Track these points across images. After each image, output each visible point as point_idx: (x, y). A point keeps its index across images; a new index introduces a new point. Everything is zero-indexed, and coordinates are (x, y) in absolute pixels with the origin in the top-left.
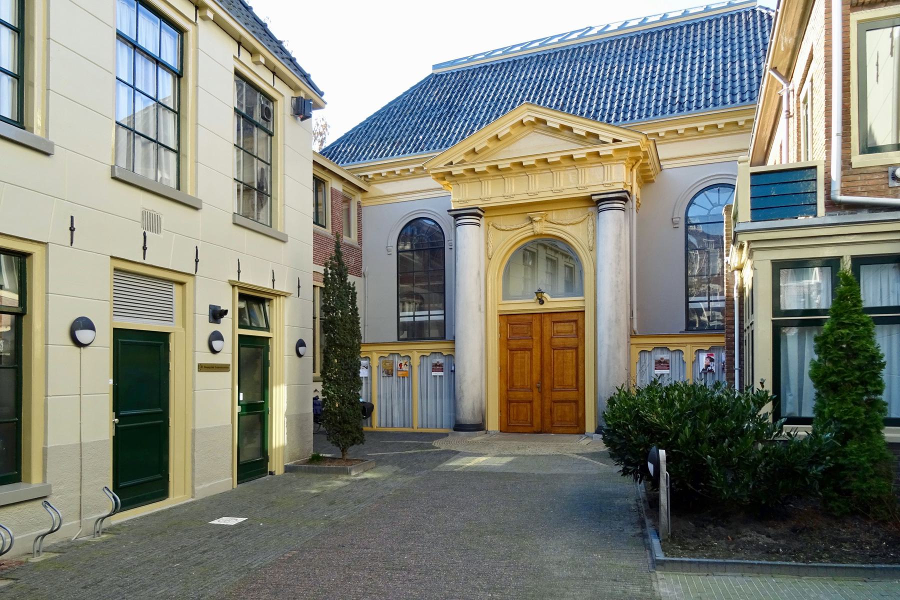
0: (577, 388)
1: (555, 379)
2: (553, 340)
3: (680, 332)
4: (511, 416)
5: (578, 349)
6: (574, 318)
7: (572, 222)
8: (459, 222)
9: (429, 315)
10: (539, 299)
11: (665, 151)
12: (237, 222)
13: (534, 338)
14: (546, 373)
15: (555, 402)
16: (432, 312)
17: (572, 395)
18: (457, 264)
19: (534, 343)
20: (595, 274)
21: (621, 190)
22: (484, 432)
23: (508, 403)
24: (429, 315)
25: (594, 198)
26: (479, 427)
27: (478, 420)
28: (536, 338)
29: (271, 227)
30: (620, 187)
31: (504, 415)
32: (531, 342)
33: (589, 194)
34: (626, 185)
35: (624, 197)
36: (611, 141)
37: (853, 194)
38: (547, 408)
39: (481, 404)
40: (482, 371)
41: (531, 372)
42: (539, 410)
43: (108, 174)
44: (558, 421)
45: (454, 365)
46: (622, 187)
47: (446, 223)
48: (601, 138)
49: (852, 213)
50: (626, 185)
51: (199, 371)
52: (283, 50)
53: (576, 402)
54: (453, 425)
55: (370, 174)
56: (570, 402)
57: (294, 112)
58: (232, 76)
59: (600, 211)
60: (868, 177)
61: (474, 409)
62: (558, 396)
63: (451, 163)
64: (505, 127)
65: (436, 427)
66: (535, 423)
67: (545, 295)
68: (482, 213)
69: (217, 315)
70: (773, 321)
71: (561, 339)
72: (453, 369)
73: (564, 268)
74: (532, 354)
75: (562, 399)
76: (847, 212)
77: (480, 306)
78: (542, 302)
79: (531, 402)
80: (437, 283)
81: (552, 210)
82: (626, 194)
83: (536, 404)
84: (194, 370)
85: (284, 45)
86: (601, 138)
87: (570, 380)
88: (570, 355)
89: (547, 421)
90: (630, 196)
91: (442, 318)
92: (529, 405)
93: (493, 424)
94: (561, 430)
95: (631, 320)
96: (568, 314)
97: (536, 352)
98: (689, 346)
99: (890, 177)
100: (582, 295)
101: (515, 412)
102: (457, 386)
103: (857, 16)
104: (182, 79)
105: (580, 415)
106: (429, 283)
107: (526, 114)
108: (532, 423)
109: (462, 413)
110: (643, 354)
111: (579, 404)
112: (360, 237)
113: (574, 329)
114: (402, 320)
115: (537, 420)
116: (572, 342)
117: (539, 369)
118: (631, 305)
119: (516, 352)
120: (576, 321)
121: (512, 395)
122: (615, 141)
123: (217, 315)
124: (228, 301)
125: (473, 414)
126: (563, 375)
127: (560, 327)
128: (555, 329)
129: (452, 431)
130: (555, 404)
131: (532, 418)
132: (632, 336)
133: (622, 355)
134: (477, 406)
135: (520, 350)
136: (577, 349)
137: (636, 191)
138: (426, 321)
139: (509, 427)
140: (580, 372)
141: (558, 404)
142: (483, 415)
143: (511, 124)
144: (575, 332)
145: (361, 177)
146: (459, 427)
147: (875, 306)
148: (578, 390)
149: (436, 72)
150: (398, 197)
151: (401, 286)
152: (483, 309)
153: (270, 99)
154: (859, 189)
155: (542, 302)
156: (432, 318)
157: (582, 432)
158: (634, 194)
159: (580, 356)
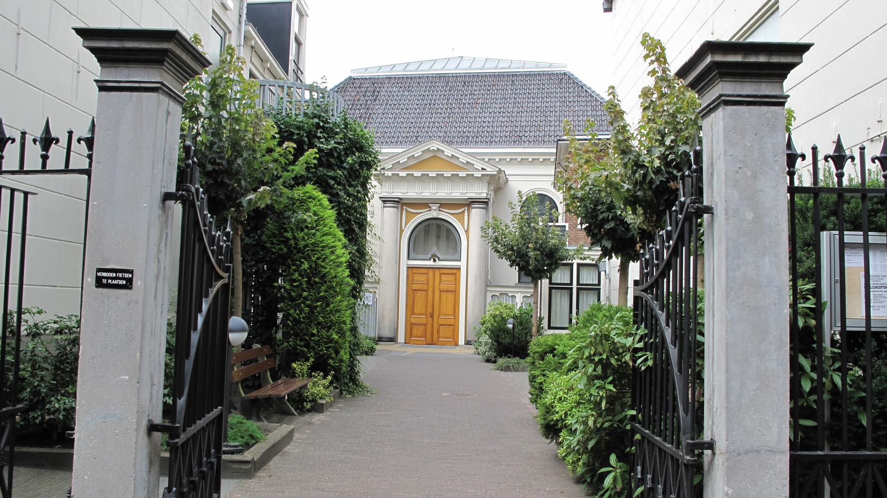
11: (508, 170)
23: (410, 328)
26: (392, 340)
30: (484, 195)
35: (485, 203)
36: (480, 169)
89: (435, 336)
93: (401, 338)
98: (519, 293)
111: (455, 327)
115: (429, 337)
121: (413, 320)
122: (483, 169)
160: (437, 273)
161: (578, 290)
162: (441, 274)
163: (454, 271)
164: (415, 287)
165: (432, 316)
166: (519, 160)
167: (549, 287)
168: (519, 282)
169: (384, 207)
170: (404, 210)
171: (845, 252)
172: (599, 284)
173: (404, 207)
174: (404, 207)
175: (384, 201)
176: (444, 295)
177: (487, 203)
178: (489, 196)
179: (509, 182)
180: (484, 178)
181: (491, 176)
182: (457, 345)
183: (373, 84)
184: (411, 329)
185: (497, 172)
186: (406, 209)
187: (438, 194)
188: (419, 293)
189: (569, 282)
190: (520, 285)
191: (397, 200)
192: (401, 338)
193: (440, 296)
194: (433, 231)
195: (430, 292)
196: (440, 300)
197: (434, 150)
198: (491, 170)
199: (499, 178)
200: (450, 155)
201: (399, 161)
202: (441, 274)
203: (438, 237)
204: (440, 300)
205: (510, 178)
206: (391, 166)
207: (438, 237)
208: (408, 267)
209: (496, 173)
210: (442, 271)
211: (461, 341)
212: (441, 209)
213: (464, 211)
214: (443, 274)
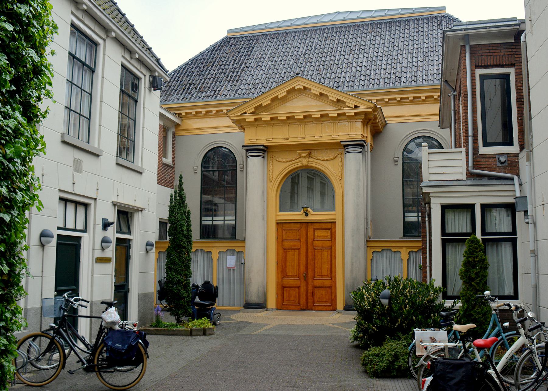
0: (331, 277)
1: (316, 271)
2: (315, 242)
3: (400, 238)
4: (285, 298)
5: (331, 249)
6: (329, 227)
7: (327, 159)
8: (347, 150)
9: (224, 220)
10: (305, 212)
11: (387, 111)
12: (119, 163)
13: (301, 240)
14: (309, 266)
15: (315, 287)
16: (226, 218)
17: (328, 283)
18: (248, 185)
19: (301, 245)
20: (343, 196)
21: (360, 139)
22: (265, 309)
23: (282, 288)
24: (224, 220)
25: (342, 143)
26: (262, 306)
27: (261, 301)
28: (303, 240)
29: (133, 162)
30: (359, 137)
31: (280, 297)
32: (299, 243)
33: (339, 141)
34: (363, 136)
35: (360, 145)
36: (353, 106)
37: (480, 169)
38: (310, 291)
39: (264, 288)
40: (264, 265)
41: (299, 266)
42: (305, 293)
43: (59, 139)
44: (318, 301)
45: (244, 259)
46: (361, 137)
47: (239, 153)
48: (347, 104)
49: (480, 179)
50: (363, 136)
51: (96, 262)
52: (152, 53)
53: (330, 287)
54: (243, 303)
55: (183, 112)
56: (326, 287)
57: (151, 85)
58: (120, 67)
59: (346, 152)
60: (487, 159)
61: (259, 292)
62: (317, 283)
63: (245, 113)
64: (283, 91)
65: (229, 305)
66: (301, 303)
67: (309, 209)
68: (266, 149)
69: (106, 225)
70: (442, 239)
71: (320, 242)
72: (243, 262)
73: (320, 184)
74: (299, 252)
75: (320, 285)
76: (477, 178)
77: (263, 216)
78: (307, 215)
79: (299, 287)
80: (231, 196)
81: (315, 150)
82: (363, 142)
83: (303, 289)
84: (93, 261)
85: (135, 27)
86: (347, 104)
87: (325, 272)
88: (326, 253)
89: (310, 301)
90: (365, 143)
91: (234, 222)
92: (297, 289)
93: (272, 302)
94: (319, 308)
95: (367, 229)
96: (325, 224)
97: (303, 251)
98: (404, 249)
99: (497, 160)
100: (334, 210)
101: (287, 294)
102: (246, 275)
103: (479, 72)
104: (95, 74)
105: (333, 297)
106: (225, 195)
107: (297, 84)
108: (299, 303)
109: (250, 296)
110: (374, 254)
111: (332, 289)
112: (174, 159)
113: (329, 234)
114: (204, 223)
115: (303, 301)
116: (328, 244)
117: (304, 263)
118: (367, 219)
119: (288, 250)
120: (330, 229)
121: (285, 282)
122: (356, 106)
123: (106, 225)
124: (112, 217)
125: (258, 296)
126: (321, 268)
127: (319, 233)
128: (316, 234)
129: (243, 308)
130: (316, 289)
131: (299, 299)
132: (367, 241)
133: (361, 254)
134: (261, 289)
135: (291, 249)
136: (331, 249)
137: (369, 140)
138: (221, 224)
139: (282, 306)
140: (333, 265)
141: (318, 289)
142: (265, 295)
143: (287, 89)
144: (329, 237)
145: (176, 114)
146: (248, 306)
147: (501, 231)
148: (332, 279)
149: (231, 35)
150: (203, 130)
151: (204, 196)
152: (265, 219)
153: (139, 79)
154: (483, 166)
155: (307, 215)
156: (226, 222)
157: (334, 309)
158: (369, 142)
159: (333, 254)
161: (444, 243)
162: (315, 229)
163: (329, 226)
164: (287, 244)
165: (306, 277)
166: (398, 99)
167: (443, 240)
168: (404, 236)
171: (489, 231)
172: (514, 232)
175: (247, 150)
177: (362, 146)
178: (365, 139)
179: (388, 125)
180: (358, 117)
181: (366, 114)
183: (249, 41)
184: (283, 293)
185: (372, 108)
187: (306, 139)
188: (291, 252)
189: (510, 230)
190: (406, 239)
191: (261, 147)
192: (272, 302)
194: (303, 182)
197: (299, 89)
198: (365, 108)
199: (376, 118)
200: (319, 94)
201: (262, 104)
202: (315, 229)
203: (310, 189)
205: (389, 121)
206: (253, 110)
207: (310, 189)
208: (277, 223)
209: (370, 110)
210: (316, 226)
211: (340, 305)
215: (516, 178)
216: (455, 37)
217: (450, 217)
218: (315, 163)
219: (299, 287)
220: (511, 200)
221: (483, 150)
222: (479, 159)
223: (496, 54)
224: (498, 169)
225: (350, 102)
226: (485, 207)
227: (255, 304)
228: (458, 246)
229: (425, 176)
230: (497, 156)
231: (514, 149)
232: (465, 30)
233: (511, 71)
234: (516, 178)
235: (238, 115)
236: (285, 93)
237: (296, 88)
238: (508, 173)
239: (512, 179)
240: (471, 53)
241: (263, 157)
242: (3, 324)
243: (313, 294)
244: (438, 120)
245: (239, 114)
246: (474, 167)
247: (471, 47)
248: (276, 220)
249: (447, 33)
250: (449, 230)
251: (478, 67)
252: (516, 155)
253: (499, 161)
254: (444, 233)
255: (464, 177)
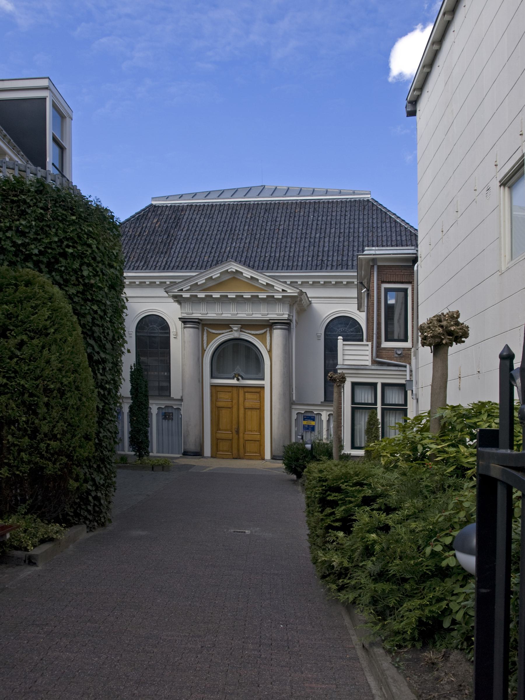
15: (246, 440)
25: (271, 321)
26: (199, 454)
27: (198, 450)
28: (235, 401)
30: (286, 316)
36: (281, 290)
62: (247, 437)
63: (182, 290)
86: (275, 288)
87: (358, 415)
89: (242, 451)
111: (261, 443)
115: (235, 451)
116: (257, 405)
121: (219, 436)
122: (283, 290)
160: (241, 392)
161: (353, 410)
163: (258, 390)
165: (238, 432)
169: (185, 328)
170: (205, 330)
172: (406, 404)
173: (205, 328)
174: (205, 328)
176: (249, 413)
178: (291, 318)
182: (263, 459)
186: (207, 331)
191: (197, 320)
192: (207, 451)
193: (245, 414)
195: (235, 410)
196: (245, 418)
197: (232, 272)
202: (245, 392)
204: (245, 418)
206: (189, 287)
209: (296, 294)
212: (242, 330)
213: (266, 332)
214: (247, 392)
215: (408, 366)
216: (365, 259)
217: (358, 391)
218: (247, 336)
219: (231, 440)
220: (403, 382)
221: (386, 345)
222: (381, 351)
223: (398, 273)
224: (395, 358)
225: (279, 287)
226: (384, 385)
227: (192, 452)
228: (363, 414)
229: (340, 361)
230: (395, 350)
231: (408, 345)
232: (374, 255)
233: (409, 287)
234: (408, 366)
235: (175, 291)
236: (219, 275)
237: (229, 271)
238: (403, 362)
239: (405, 367)
240: (378, 269)
241: (198, 328)
242: (5, 472)
243: (244, 447)
244: (356, 296)
245: (176, 291)
246: (378, 356)
247: (379, 267)
248: (210, 383)
249: (359, 256)
250: (357, 400)
251: (383, 282)
252: (409, 349)
253: (396, 353)
254: (353, 402)
255: (369, 363)
